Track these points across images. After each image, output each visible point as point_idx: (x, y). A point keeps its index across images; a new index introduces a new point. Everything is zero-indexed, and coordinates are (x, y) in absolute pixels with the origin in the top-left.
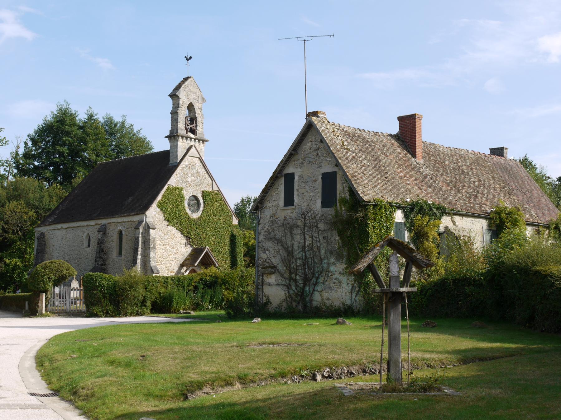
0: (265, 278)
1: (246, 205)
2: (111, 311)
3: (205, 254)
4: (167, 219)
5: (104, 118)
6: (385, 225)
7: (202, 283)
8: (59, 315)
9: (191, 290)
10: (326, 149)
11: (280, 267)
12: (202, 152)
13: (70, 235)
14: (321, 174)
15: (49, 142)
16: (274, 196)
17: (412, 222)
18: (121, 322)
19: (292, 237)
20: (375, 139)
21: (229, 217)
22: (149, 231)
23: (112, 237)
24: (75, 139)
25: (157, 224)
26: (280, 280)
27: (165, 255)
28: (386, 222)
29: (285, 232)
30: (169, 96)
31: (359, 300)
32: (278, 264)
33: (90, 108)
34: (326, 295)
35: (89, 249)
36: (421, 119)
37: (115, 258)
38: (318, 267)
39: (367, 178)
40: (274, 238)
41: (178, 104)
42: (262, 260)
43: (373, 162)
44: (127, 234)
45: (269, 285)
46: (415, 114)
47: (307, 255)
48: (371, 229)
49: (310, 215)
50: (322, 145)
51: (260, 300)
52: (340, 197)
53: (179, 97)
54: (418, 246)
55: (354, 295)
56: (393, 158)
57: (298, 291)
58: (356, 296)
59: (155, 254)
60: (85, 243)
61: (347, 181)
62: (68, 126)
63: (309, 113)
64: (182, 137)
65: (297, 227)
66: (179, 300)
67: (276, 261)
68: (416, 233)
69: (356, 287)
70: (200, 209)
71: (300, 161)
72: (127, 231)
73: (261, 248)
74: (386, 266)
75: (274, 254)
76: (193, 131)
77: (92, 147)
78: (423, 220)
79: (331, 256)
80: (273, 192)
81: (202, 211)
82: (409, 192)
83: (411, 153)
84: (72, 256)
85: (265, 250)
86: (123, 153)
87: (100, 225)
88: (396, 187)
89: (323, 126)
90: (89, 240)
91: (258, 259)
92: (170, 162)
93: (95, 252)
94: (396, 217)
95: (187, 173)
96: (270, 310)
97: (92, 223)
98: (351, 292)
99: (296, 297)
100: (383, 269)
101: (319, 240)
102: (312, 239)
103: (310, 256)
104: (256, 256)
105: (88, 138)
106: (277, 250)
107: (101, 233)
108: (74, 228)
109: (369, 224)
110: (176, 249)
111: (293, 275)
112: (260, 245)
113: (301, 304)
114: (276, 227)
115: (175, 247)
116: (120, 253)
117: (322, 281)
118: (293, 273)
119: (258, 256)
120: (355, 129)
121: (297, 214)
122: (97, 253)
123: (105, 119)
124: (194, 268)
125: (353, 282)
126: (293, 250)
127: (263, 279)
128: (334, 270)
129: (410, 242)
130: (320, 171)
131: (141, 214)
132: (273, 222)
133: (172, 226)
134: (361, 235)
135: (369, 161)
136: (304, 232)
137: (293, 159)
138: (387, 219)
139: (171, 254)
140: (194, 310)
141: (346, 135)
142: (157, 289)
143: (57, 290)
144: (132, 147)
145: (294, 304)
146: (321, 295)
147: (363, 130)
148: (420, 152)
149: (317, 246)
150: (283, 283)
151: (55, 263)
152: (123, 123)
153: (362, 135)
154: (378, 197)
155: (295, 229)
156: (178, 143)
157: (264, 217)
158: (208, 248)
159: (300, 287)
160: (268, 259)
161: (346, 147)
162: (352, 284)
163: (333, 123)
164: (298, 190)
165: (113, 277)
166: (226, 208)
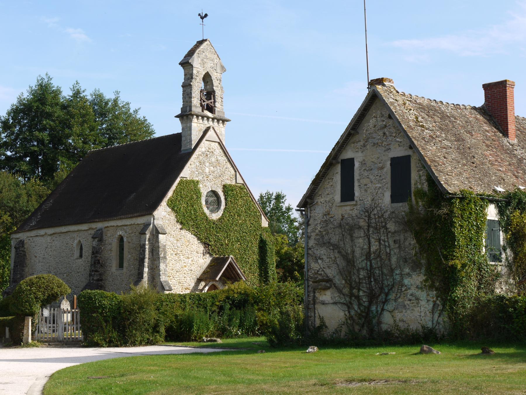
0: (317, 295)
1: (265, 203)
2: (115, 339)
3: (228, 266)
4: (180, 221)
5: (92, 95)
6: (475, 223)
7: (228, 302)
8: (49, 345)
9: (214, 311)
10: (396, 126)
11: (337, 281)
12: (222, 135)
13: (56, 242)
14: (390, 159)
15: (25, 125)
16: (327, 188)
17: (508, 219)
18: (131, 353)
19: (352, 241)
20: (456, 114)
21: (257, 217)
22: (158, 237)
23: (111, 244)
24: (57, 122)
25: (168, 227)
26: (338, 297)
27: (178, 266)
28: (476, 220)
29: (343, 235)
30: (180, 64)
31: (444, 322)
32: (334, 277)
33: (77, 83)
34: (398, 316)
35: (81, 260)
36: (513, 87)
37: (115, 271)
38: (387, 280)
39: (449, 163)
40: (329, 243)
41: (192, 75)
42: (313, 272)
43: (456, 143)
44: (130, 241)
45: (323, 303)
46: (506, 81)
47: (373, 265)
48: (458, 229)
49: (375, 212)
50: (391, 122)
51: (312, 323)
52: (415, 188)
53: (192, 66)
54: (516, 250)
55: (436, 315)
56: (480, 137)
57: (362, 311)
58: (439, 316)
59: (166, 266)
60: (75, 253)
61: (425, 168)
62: (49, 105)
63: (371, 81)
64: (198, 116)
65: (358, 228)
66: (201, 324)
67: (331, 272)
68: (513, 234)
69: (439, 305)
70: (220, 207)
71: (362, 143)
72: (130, 237)
73: (312, 256)
74: (477, 277)
75: (329, 264)
76: (211, 109)
77: (78, 132)
78: (523, 218)
79: (404, 265)
80: (326, 184)
81: (223, 210)
82: (502, 181)
83: (502, 130)
84: (60, 270)
85: (316, 259)
86: (117, 139)
87: (95, 230)
88: (486, 174)
89: (391, 98)
90: (81, 249)
91: (308, 271)
92: (182, 149)
93: (89, 265)
94: (488, 213)
95: (204, 163)
96: (325, 335)
97: (84, 227)
98: (433, 312)
99: (360, 319)
100: (473, 281)
101: (389, 244)
102: (380, 243)
103: (377, 266)
104: (306, 266)
105: (73, 121)
106: (333, 259)
107: (96, 240)
108: (61, 235)
109: (455, 222)
110: (192, 259)
111: (355, 291)
112: (310, 252)
113: (365, 328)
114: (331, 228)
115: (190, 256)
116: (121, 265)
117: (393, 298)
118: (354, 288)
119: (308, 266)
120: (430, 100)
121: (358, 212)
122: (91, 265)
123: (94, 97)
124: (214, 283)
125: (435, 299)
126: (355, 257)
127: (314, 296)
128: (409, 284)
129: (505, 245)
130: (388, 155)
131: (148, 215)
132: (326, 222)
133: (187, 230)
134: (445, 237)
135: (451, 141)
136: (369, 235)
137: (351, 141)
138: (477, 216)
139: (185, 266)
140: (219, 336)
141: (420, 108)
142: (172, 310)
143: (46, 313)
144: (127, 130)
145: (357, 328)
146: (393, 316)
147: (441, 101)
148: (513, 129)
149: (386, 252)
150: (342, 301)
151: (43, 278)
152: (116, 101)
153: (440, 108)
154: (465, 187)
155: (356, 231)
156: (193, 124)
157: (315, 216)
158: (232, 258)
159: (365, 306)
160: (321, 270)
161: (421, 124)
162: (434, 301)
163: (402, 94)
164: (359, 180)
165: (117, 295)
166: (253, 206)
